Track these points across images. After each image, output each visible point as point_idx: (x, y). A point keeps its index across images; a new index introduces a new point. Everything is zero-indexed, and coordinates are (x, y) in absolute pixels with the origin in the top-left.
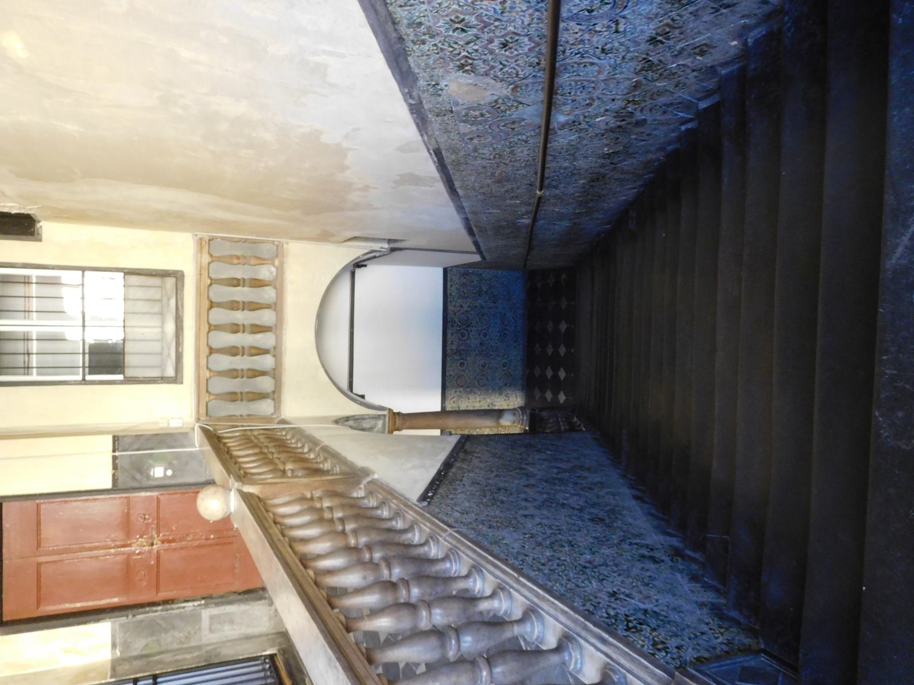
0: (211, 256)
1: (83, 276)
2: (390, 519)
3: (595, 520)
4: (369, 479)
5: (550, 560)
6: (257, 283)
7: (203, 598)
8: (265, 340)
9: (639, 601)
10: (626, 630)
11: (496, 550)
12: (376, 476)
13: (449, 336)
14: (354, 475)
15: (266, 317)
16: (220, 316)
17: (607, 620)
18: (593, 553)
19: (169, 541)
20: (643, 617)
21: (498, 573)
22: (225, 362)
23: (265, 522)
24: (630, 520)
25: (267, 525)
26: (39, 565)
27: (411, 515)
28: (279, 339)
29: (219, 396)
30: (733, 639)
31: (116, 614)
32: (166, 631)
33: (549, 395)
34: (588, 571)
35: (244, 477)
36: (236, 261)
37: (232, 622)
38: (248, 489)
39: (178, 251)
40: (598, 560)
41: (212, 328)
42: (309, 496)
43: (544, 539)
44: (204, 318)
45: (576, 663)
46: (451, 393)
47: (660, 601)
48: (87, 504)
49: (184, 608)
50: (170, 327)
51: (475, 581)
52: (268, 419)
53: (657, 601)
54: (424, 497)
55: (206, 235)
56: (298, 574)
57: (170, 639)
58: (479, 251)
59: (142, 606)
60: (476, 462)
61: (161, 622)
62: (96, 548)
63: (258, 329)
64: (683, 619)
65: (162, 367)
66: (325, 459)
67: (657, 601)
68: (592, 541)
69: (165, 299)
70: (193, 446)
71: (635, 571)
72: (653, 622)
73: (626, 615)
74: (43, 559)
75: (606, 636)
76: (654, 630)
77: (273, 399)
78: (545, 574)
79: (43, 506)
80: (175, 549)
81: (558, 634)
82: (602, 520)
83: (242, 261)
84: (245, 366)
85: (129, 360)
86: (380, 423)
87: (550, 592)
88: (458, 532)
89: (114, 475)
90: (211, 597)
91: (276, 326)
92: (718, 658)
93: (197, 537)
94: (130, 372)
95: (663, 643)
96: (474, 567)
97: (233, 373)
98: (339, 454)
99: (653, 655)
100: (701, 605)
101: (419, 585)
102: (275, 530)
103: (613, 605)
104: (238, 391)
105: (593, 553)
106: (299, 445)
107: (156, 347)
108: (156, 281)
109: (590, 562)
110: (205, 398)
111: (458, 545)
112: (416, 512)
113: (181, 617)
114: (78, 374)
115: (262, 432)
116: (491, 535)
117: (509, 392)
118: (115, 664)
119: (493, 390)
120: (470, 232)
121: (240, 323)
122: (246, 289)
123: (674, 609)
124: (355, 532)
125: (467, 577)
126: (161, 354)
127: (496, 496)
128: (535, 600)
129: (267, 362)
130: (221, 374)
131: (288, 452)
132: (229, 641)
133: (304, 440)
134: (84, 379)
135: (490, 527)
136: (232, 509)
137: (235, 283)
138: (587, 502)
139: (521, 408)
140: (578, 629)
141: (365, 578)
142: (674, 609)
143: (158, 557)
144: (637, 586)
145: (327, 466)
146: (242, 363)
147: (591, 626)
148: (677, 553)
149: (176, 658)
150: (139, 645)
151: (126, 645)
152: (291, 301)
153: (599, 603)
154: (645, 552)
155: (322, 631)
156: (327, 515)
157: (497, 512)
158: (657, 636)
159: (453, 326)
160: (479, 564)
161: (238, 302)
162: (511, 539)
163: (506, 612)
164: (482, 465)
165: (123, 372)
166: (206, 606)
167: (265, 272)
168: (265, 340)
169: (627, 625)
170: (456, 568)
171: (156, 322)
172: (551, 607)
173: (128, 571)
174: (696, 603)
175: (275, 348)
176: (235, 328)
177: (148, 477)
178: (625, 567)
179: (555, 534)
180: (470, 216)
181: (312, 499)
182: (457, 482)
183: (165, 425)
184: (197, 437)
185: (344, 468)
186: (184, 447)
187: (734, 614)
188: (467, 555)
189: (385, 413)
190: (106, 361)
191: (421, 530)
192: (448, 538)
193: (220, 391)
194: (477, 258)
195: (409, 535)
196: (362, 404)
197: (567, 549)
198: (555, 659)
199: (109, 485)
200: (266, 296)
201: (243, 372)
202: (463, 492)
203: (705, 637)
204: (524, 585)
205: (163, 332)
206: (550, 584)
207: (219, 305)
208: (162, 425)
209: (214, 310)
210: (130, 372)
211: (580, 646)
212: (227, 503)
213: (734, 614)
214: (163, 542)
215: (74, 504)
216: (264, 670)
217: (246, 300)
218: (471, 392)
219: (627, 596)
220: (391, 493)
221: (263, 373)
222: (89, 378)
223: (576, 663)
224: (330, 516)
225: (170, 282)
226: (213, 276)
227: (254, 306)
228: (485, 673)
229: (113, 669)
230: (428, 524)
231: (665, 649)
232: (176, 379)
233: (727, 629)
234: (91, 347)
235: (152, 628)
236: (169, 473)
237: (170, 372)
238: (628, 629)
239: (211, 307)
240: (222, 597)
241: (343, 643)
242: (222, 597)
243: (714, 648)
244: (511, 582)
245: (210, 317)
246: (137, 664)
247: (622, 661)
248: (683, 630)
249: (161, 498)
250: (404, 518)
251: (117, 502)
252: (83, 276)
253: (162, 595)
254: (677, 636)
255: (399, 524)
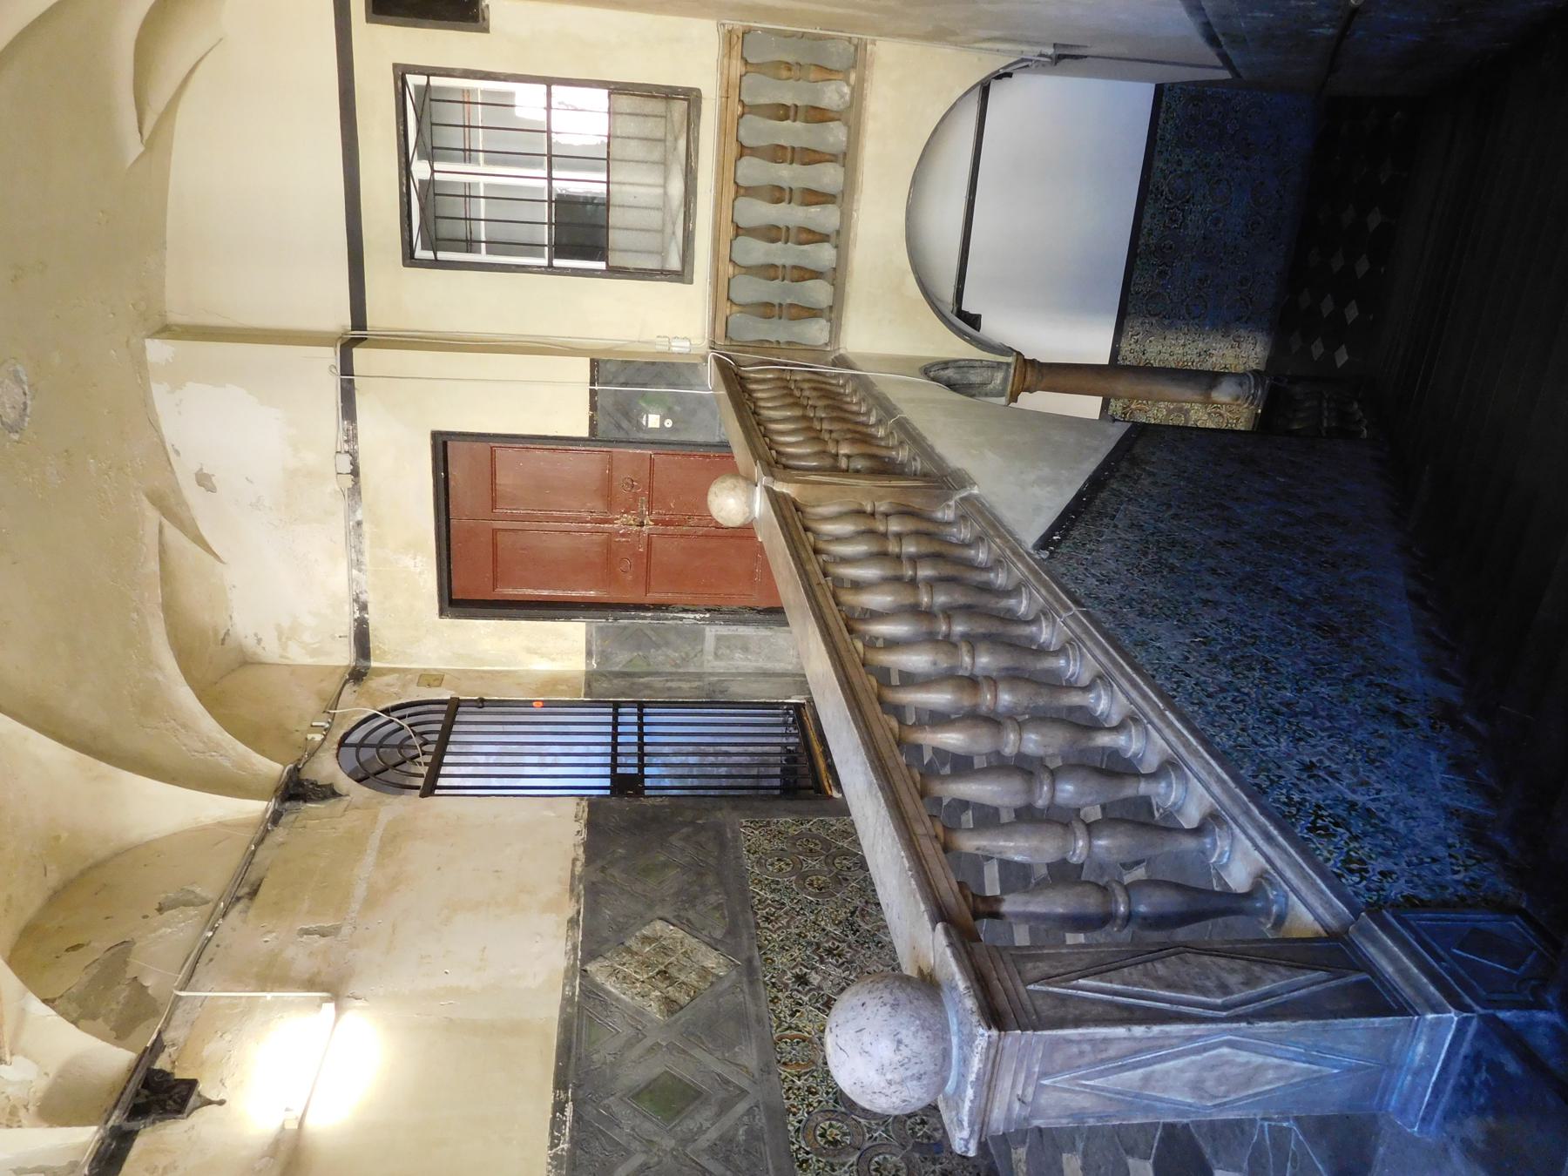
0: (746, 62)
1: (549, 94)
2: (987, 569)
3: (1325, 628)
4: (964, 494)
5: (1222, 690)
6: (818, 115)
7: (708, 611)
8: (823, 217)
9: (1348, 786)
10: (1310, 830)
11: (1141, 656)
12: (975, 491)
13: (1147, 219)
14: (942, 481)
15: (828, 177)
16: (755, 171)
17: (1286, 809)
18: (1299, 691)
19: (666, 523)
20: (1344, 814)
21: (1134, 694)
22: (757, 251)
23: (800, 548)
24: (1385, 638)
25: (804, 555)
26: (495, 531)
27: (1019, 571)
28: (846, 217)
29: (745, 307)
30: (1483, 880)
31: (591, 613)
32: (658, 647)
33: (1318, 350)
34: (1280, 719)
35: (777, 464)
36: (785, 73)
37: (745, 649)
38: (780, 487)
39: (691, 54)
40: (1304, 703)
41: (742, 191)
42: (869, 508)
43: (1224, 651)
44: (729, 175)
45: (1221, 855)
46: (1134, 325)
47: (1384, 794)
48: (557, 455)
49: (681, 619)
50: (676, 187)
51: (1099, 698)
52: (816, 352)
53: (1379, 792)
54: (1045, 542)
55: (738, 25)
56: (841, 646)
57: (663, 658)
58: (1227, 63)
59: (625, 607)
60: (1146, 481)
61: (649, 632)
62: (567, 519)
63: (814, 199)
64: (1411, 831)
65: (662, 253)
66: (901, 443)
67: (1379, 792)
68: (1303, 666)
69: (670, 138)
70: (704, 385)
71: (1360, 735)
72: (1358, 826)
73: (1319, 807)
74: (498, 525)
75: (1275, 833)
76: (1355, 838)
77: (830, 320)
78: (1208, 713)
79: (498, 452)
80: (672, 536)
81: (1205, 809)
82: (1335, 630)
83: (796, 72)
84: (789, 262)
85: (615, 238)
86: (999, 376)
87: (1207, 743)
88: (1087, 614)
89: (591, 419)
90: (719, 611)
91: (843, 192)
92: (1445, 905)
93: (704, 523)
94: (616, 259)
95: (1361, 861)
96: (1100, 677)
97: (769, 271)
98: (924, 439)
99: (1339, 876)
100: (1451, 813)
101: (1012, 691)
102: (814, 567)
103: (1304, 787)
104: (776, 301)
105: (1299, 691)
106: (863, 409)
107: (654, 219)
108: (656, 106)
109: (1288, 705)
110: (726, 308)
111: (1083, 636)
112: (1027, 565)
113: (678, 631)
114: (542, 256)
115: (808, 376)
116: (1138, 628)
117: (1242, 332)
118: (591, 678)
119: (1214, 327)
120: (1212, 40)
121: (784, 185)
122: (799, 125)
123: (1403, 811)
124: (932, 583)
125: (1087, 689)
126: (662, 231)
127: (1165, 554)
128: (1182, 750)
129: (824, 255)
130: (750, 270)
131: (844, 420)
132: (740, 674)
133: (870, 401)
134: (551, 265)
135: (1141, 613)
136: (757, 514)
137: (783, 112)
138: (1318, 591)
139: (1256, 373)
140: (1236, 811)
141: (935, 664)
142: (1403, 811)
143: (649, 544)
144: (1353, 761)
145: (902, 455)
146: (783, 254)
147: (1256, 811)
148: (1447, 715)
149: (669, 684)
150: (621, 659)
151: (605, 657)
152: (871, 151)
153: (1281, 777)
154: (1389, 702)
155: (864, 743)
156: (893, 548)
157: (1160, 588)
158: (1356, 850)
159: (1156, 201)
160: (1109, 674)
161: (783, 147)
162: (1170, 642)
163: (1135, 755)
164: (1155, 491)
165: (604, 258)
166: (712, 621)
167: (833, 95)
168: (823, 217)
169: (1314, 822)
170: (1076, 667)
171: (655, 178)
172: (1200, 762)
173: (608, 558)
174: (1445, 807)
175: (838, 232)
176: (777, 194)
177: (639, 427)
178: (1345, 723)
179: (1246, 644)
180: (1212, 20)
181: (873, 514)
182: (1106, 521)
183: (665, 349)
184: (710, 373)
185: (929, 467)
186: (690, 386)
187: (1504, 841)
188: (1094, 656)
189: (1010, 360)
190: (580, 233)
191: (1031, 597)
192: (1069, 622)
193: (749, 300)
194: (1225, 75)
195: (1012, 602)
196: (974, 341)
197: (1257, 674)
198: (1189, 843)
199: (584, 432)
200: (831, 139)
201: (784, 267)
202: (1111, 541)
203: (1436, 867)
204: (1170, 725)
205: (665, 193)
206: (1212, 731)
207: (754, 152)
208: (660, 348)
209: (745, 160)
210: (616, 259)
211: (1233, 836)
212: (750, 503)
213: (1504, 841)
214: (656, 523)
215: (538, 452)
216: (785, 724)
217: (796, 145)
218: (1169, 327)
219: (1333, 774)
220: (993, 526)
221: (816, 275)
222: (557, 263)
223: (1221, 855)
224: (897, 550)
225: (679, 107)
226: (747, 100)
227: (809, 157)
228: (1081, 843)
229: (588, 684)
230: (1043, 592)
231: (1362, 872)
232: (682, 275)
233: (1479, 861)
234: (559, 195)
235: (638, 640)
236: (669, 423)
237: (674, 263)
238: (1313, 829)
239: (737, 235)
240: (733, 612)
241: (891, 764)
242: (733, 612)
243: (1444, 887)
244: (1151, 714)
245: (739, 173)
246: (621, 683)
247: (1289, 874)
248: (1404, 848)
249: (656, 458)
250: (1009, 572)
251: (598, 456)
252: (549, 94)
253: (653, 597)
254: (1387, 854)
255: (1000, 579)
